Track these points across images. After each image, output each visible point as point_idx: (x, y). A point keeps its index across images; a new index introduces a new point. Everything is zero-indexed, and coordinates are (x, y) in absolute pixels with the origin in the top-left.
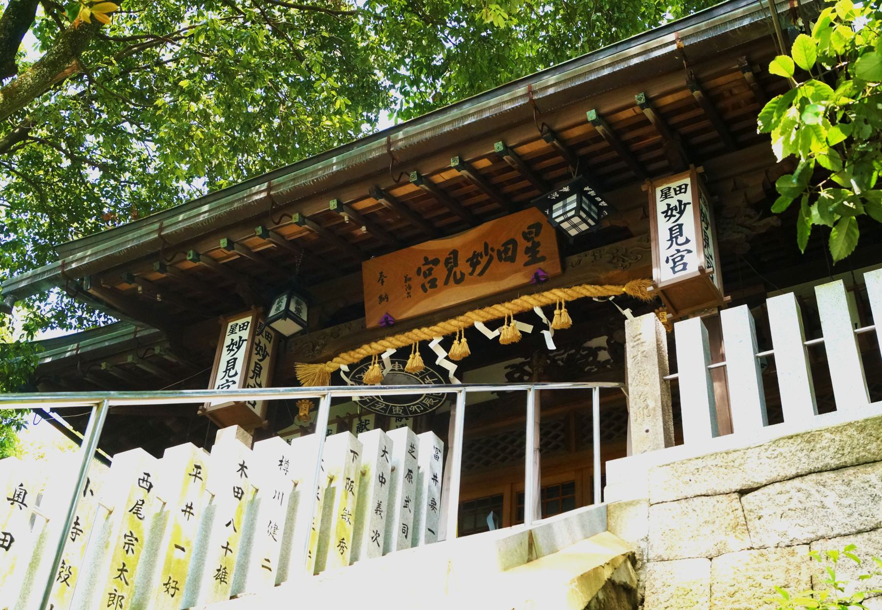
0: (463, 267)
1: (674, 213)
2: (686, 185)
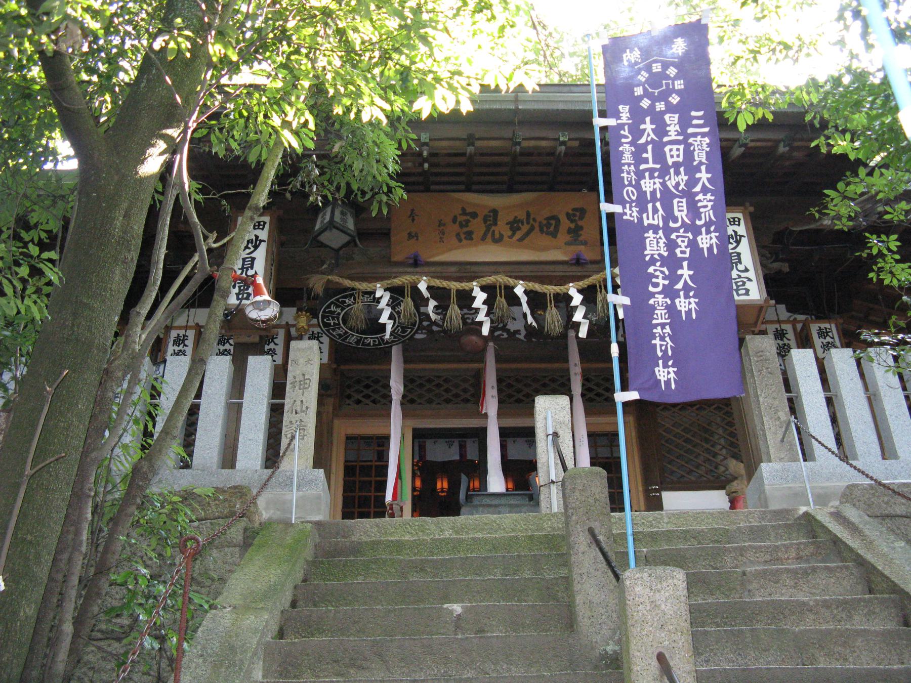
0: (502, 227)
1: (250, 245)
2: (265, 223)
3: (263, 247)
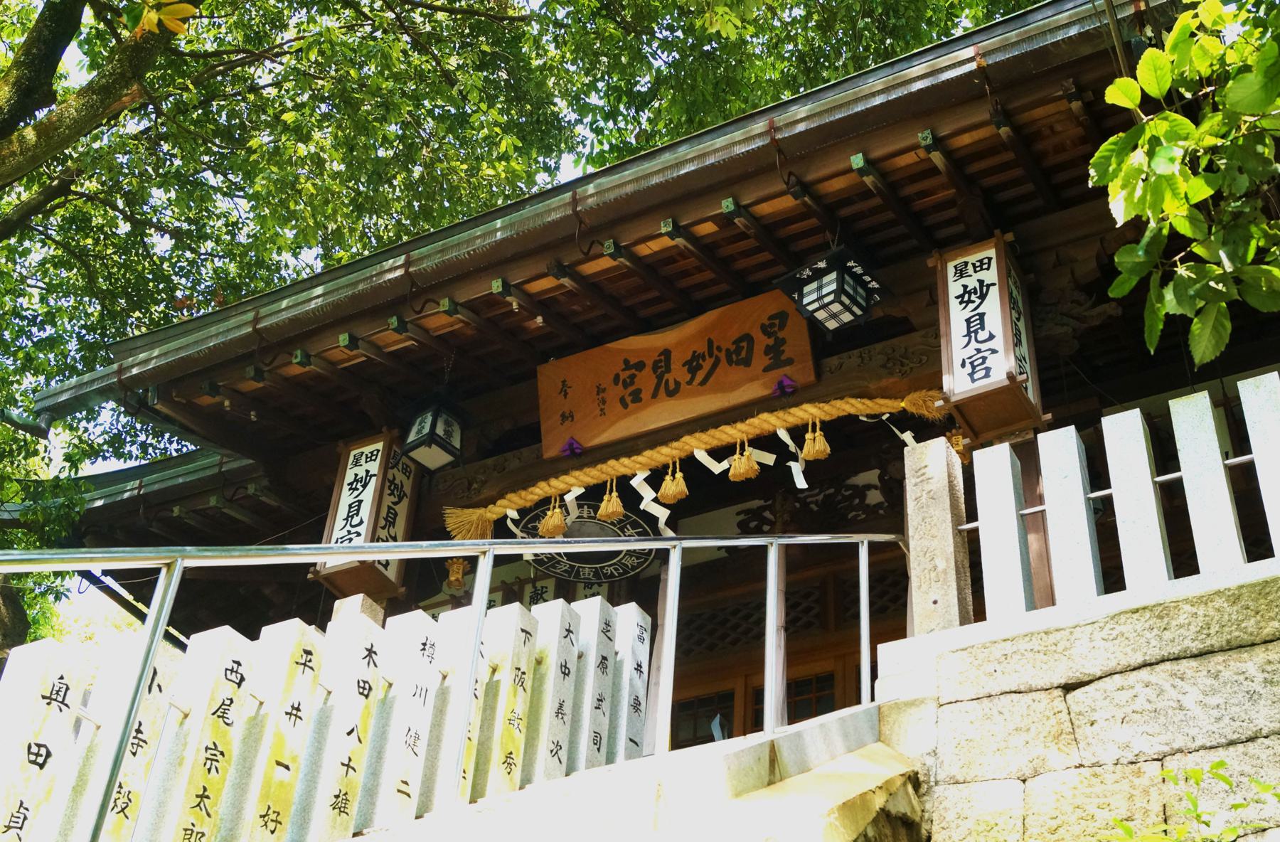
0: (678, 372)
1: (973, 297)
2: (990, 259)
3: (994, 293)
